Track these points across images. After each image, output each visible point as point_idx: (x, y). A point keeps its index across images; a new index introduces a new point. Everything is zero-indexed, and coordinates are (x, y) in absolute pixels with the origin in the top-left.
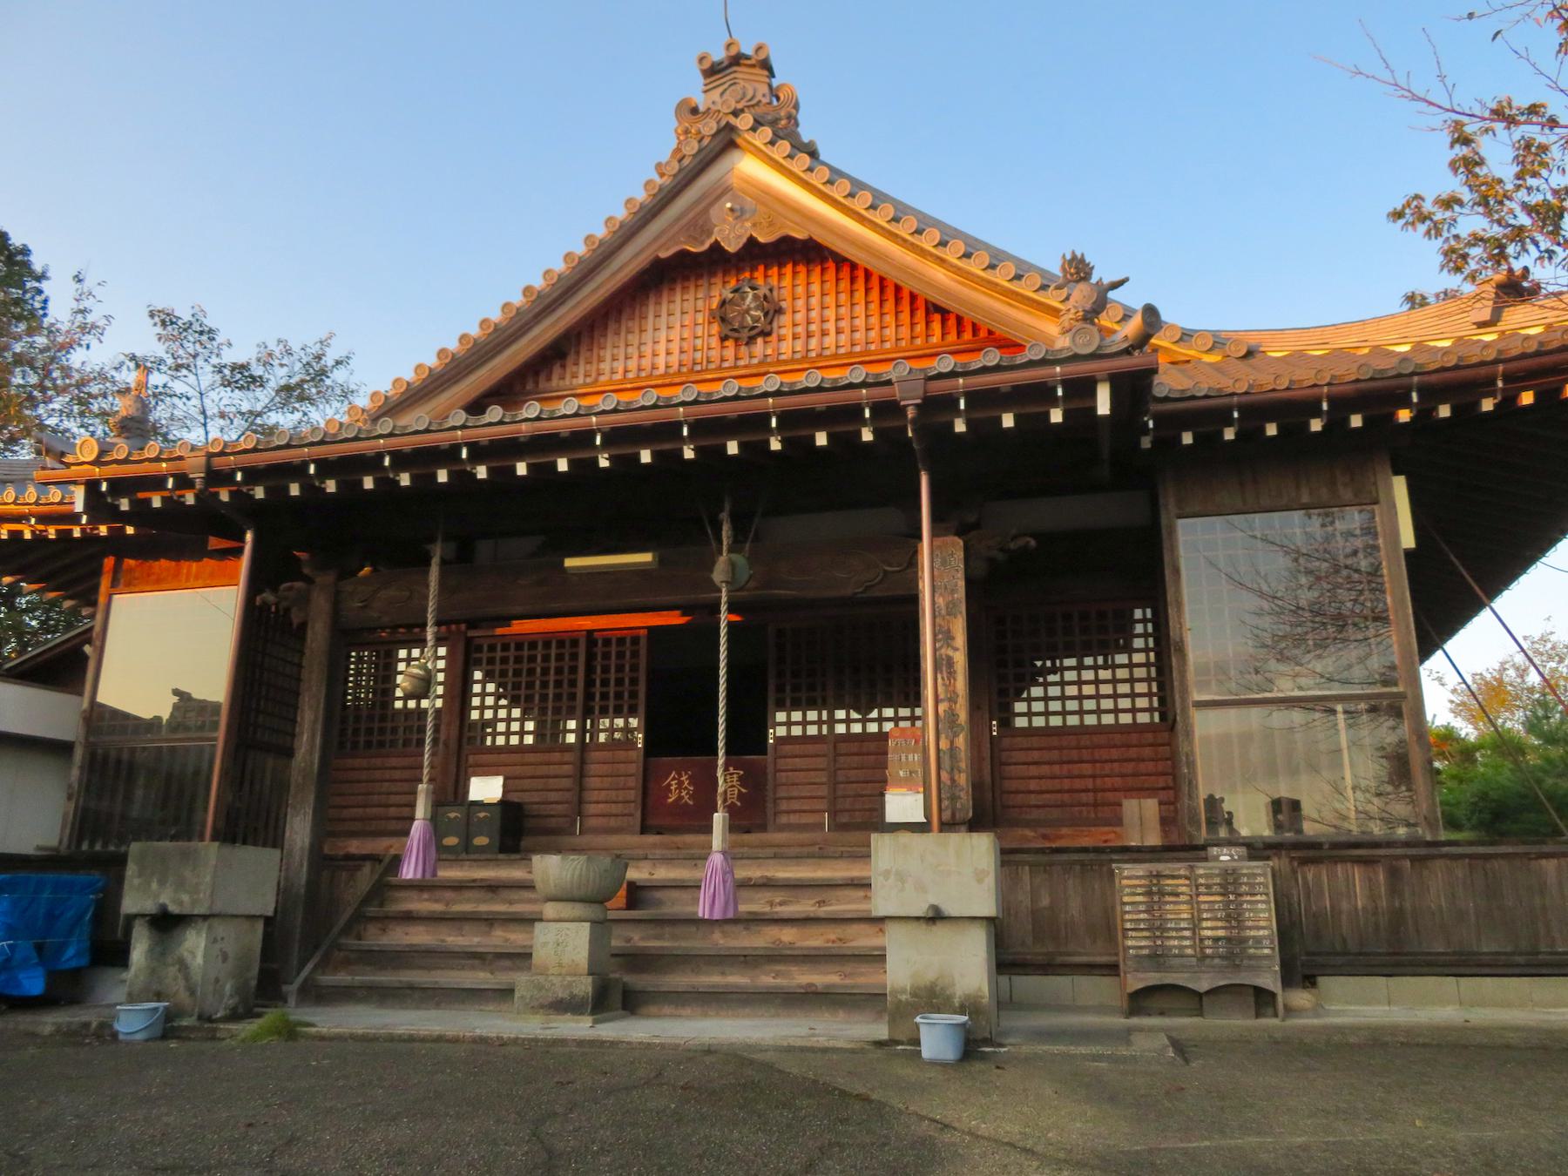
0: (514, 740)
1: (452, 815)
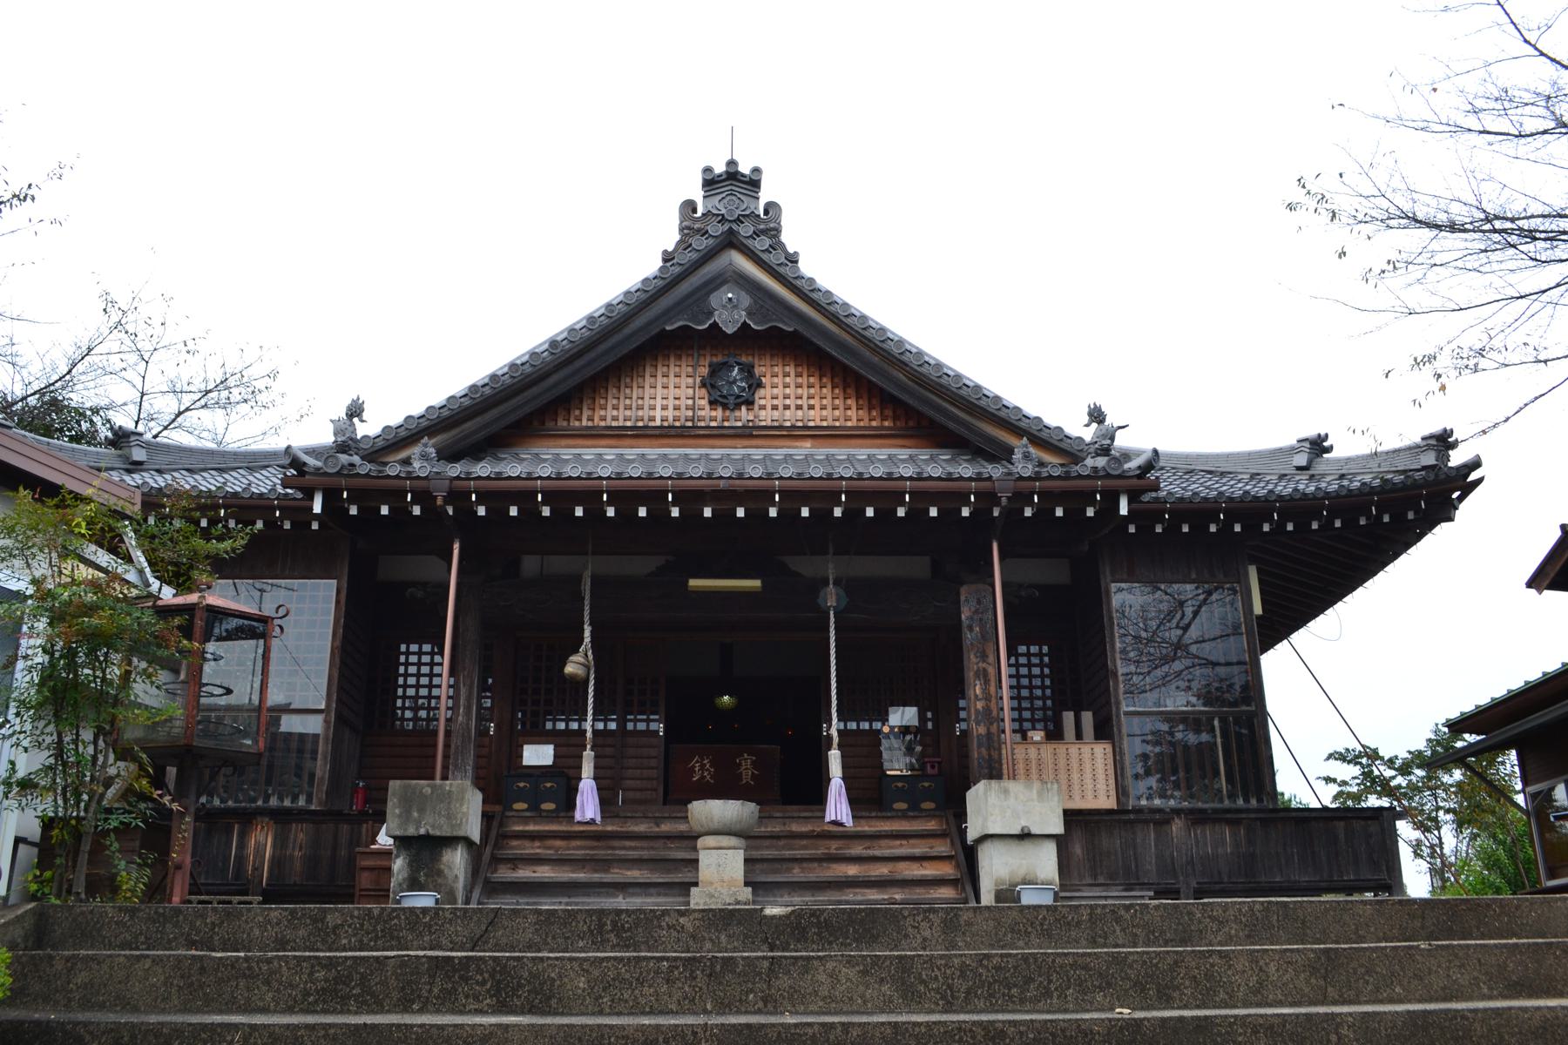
1: (522, 785)
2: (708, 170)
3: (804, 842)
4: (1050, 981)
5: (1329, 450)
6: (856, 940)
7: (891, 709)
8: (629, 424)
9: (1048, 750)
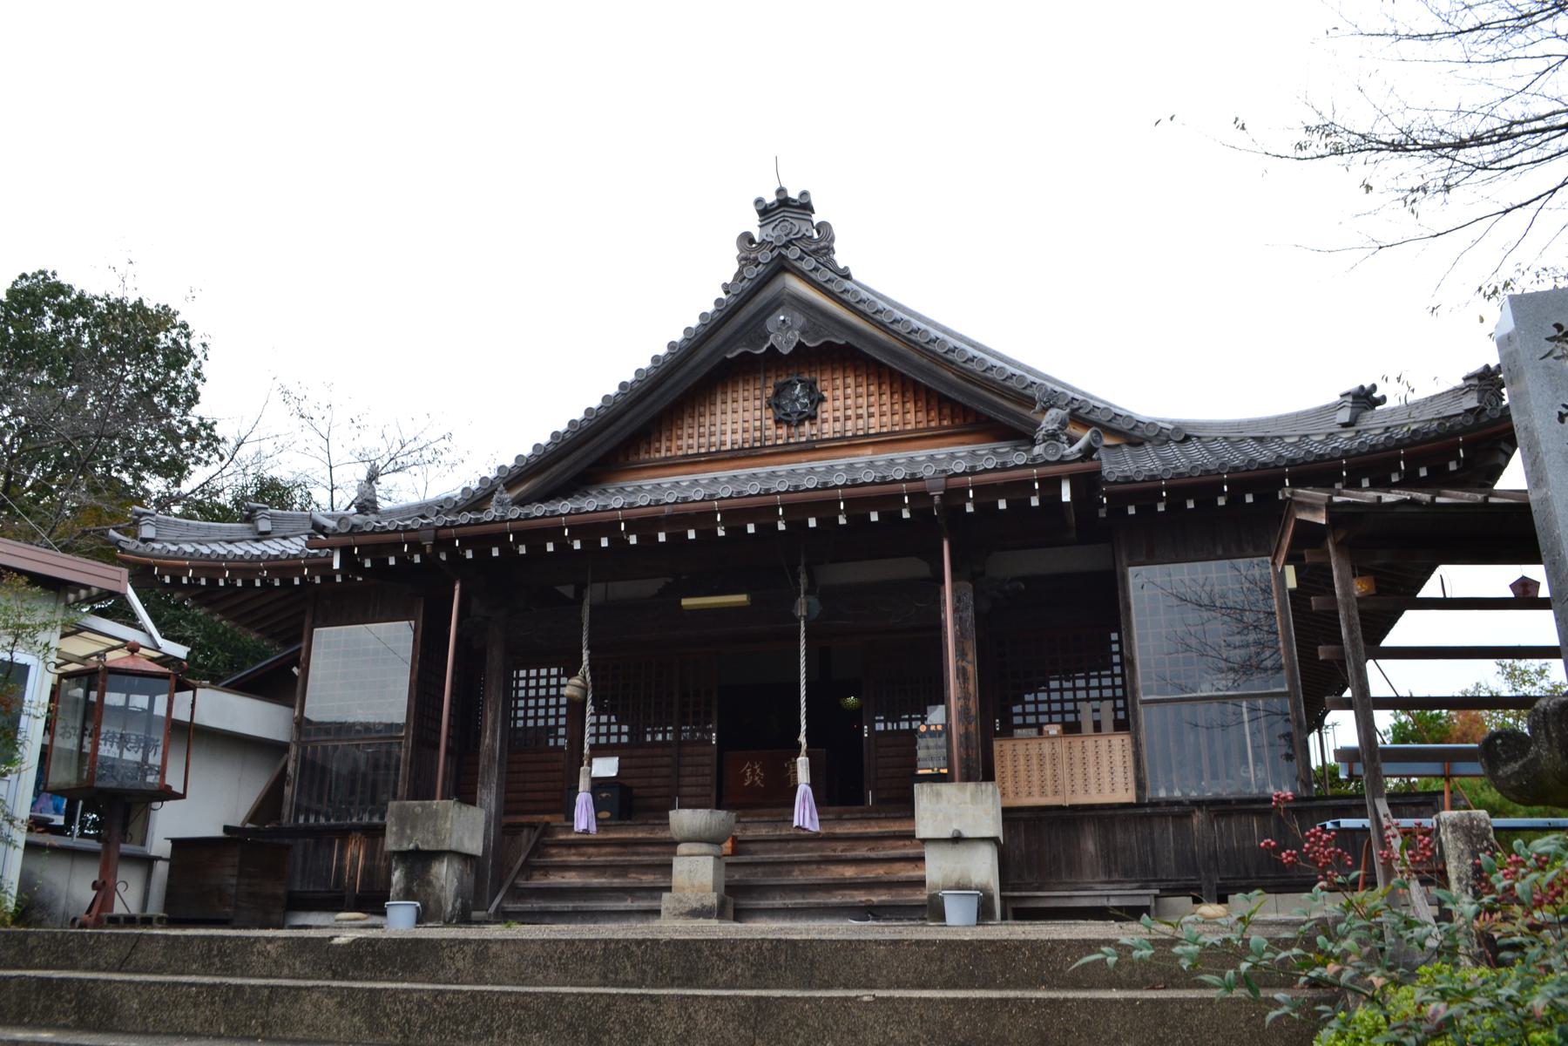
0: (614, 739)
2: (758, 201)
3: (811, 845)
4: (493, 1020)
5: (1383, 400)
6: (402, 969)
7: (929, 708)
8: (703, 450)
9: (1062, 745)
